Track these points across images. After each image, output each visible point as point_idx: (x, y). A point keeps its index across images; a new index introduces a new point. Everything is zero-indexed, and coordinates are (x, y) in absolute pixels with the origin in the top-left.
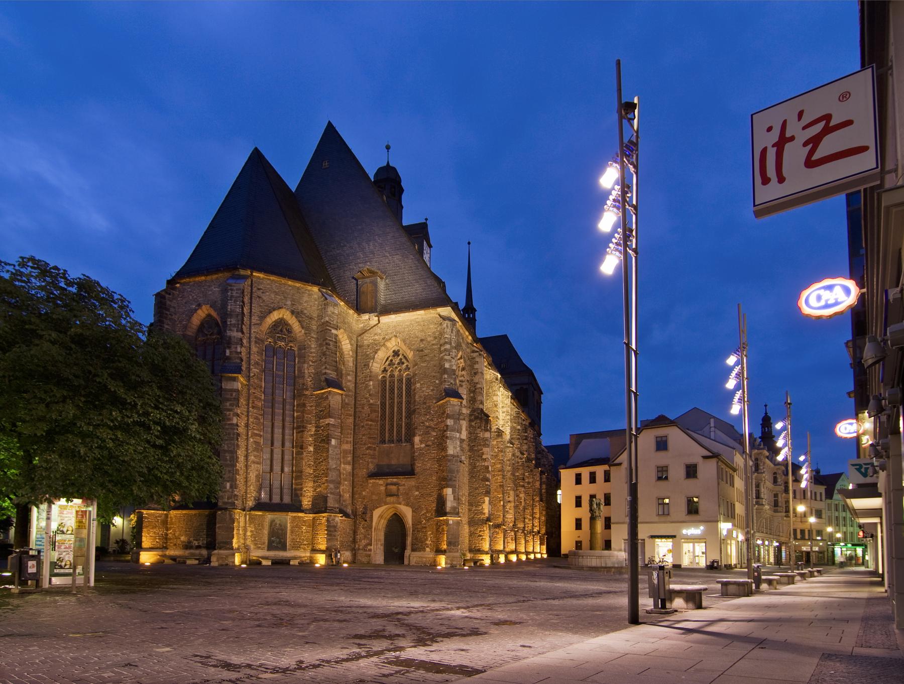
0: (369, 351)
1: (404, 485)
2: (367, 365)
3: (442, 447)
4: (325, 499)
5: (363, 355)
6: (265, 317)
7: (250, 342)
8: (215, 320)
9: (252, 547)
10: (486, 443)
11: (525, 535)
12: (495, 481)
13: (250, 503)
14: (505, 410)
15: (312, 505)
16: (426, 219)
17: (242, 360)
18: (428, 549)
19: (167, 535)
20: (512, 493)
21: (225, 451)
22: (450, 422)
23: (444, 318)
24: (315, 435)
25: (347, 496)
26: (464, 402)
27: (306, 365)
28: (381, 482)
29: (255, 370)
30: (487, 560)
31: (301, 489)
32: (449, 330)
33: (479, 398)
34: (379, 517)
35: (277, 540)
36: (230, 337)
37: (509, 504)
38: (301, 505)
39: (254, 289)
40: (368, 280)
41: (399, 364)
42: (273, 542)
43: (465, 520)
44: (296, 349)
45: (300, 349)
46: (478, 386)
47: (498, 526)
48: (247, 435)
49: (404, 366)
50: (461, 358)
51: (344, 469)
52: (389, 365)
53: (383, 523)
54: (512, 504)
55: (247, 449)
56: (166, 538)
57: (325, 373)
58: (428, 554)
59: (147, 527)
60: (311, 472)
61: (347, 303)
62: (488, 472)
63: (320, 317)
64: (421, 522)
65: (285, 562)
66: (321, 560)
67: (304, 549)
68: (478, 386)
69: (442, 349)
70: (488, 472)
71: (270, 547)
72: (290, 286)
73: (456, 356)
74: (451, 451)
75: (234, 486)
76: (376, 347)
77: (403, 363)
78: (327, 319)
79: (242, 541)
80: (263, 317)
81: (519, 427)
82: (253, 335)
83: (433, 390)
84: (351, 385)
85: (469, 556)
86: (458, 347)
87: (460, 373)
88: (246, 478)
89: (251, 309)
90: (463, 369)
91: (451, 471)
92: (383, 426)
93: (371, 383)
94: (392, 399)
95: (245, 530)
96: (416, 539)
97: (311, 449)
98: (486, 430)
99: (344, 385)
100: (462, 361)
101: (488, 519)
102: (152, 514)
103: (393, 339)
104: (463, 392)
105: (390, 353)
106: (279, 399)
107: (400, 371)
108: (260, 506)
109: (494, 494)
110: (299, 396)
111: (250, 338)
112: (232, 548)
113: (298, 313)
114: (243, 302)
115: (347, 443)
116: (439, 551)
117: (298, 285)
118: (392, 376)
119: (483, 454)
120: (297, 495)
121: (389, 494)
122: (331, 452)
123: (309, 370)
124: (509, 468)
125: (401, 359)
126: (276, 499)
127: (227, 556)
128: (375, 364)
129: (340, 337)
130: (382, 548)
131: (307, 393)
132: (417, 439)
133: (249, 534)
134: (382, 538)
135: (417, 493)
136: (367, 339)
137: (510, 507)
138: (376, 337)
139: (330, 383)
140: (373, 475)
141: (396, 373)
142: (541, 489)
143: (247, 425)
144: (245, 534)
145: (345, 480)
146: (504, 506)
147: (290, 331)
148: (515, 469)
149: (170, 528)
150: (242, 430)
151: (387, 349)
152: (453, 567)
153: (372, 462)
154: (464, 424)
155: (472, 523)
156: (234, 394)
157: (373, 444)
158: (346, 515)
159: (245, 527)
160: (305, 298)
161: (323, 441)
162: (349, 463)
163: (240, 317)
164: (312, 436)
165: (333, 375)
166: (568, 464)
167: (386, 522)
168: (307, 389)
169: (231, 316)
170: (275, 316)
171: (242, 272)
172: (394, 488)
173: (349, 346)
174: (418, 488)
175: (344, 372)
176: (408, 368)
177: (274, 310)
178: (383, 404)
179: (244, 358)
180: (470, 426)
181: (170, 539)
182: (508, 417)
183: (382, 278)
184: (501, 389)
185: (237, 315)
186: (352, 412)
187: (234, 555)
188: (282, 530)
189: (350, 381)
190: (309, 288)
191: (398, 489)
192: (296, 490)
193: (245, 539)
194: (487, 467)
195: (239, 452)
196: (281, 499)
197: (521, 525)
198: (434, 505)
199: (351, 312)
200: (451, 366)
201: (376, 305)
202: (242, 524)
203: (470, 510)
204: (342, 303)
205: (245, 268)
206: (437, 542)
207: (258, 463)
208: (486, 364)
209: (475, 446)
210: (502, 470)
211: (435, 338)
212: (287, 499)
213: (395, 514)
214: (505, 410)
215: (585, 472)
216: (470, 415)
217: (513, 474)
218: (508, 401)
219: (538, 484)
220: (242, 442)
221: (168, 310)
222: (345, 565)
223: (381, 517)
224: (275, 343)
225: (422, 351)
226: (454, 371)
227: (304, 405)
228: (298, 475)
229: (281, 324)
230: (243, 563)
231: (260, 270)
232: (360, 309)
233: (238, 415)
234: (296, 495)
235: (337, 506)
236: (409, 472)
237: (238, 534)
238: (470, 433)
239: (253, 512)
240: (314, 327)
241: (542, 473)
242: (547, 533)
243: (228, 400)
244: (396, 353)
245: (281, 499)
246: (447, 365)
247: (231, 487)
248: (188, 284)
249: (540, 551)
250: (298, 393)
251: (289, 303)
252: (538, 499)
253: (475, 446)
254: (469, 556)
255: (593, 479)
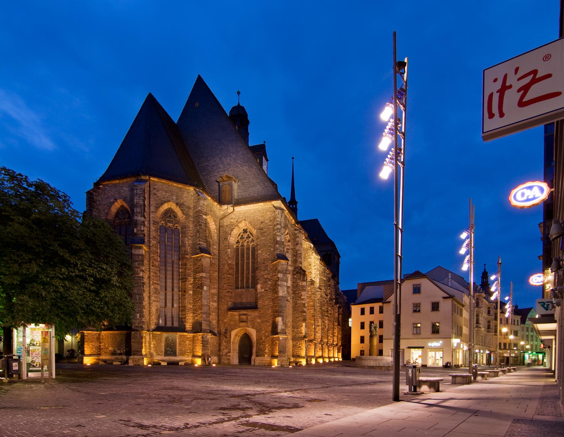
0: (228, 230)
1: (251, 315)
2: (226, 239)
3: (277, 292)
4: (200, 324)
5: (223, 232)
6: (159, 207)
7: (149, 224)
8: (126, 209)
9: (155, 354)
10: (303, 289)
11: (328, 347)
12: (309, 313)
13: (153, 327)
14: (316, 267)
15: (192, 328)
16: (265, 142)
17: (145, 236)
18: (266, 355)
19: (100, 346)
20: (320, 320)
21: (136, 294)
22: (280, 275)
23: (276, 208)
24: (193, 283)
25: (214, 322)
26: (290, 263)
27: (186, 239)
28: (236, 313)
29: (153, 242)
30: (304, 362)
31: (185, 318)
32: (279, 216)
33: (299, 260)
34: (235, 335)
35: (170, 349)
36: (136, 220)
37: (318, 327)
38: (185, 328)
39: (152, 189)
40: (226, 183)
41: (247, 238)
42: (168, 351)
43: (290, 337)
44: (179, 228)
45: (182, 228)
46: (299, 252)
47: (311, 341)
48: (150, 284)
49: (250, 239)
50: (287, 234)
51: (212, 305)
52: (241, 238)
53: (238, 339)
54: (320, 327)
55: (150, 293)
56: (99, 348)
57: (199, 244)
58: (267, 358)
59: (87, 341)
60: (191, 307)
61: (213, 198)
62: (305, 307)
63: (195, 207)
64: (262, 339)
65: (176, 363)
66: (199, 362)
67: (188, 355)
68: (299, 252)
69: (275, 228)
70: (305, 307)
71: (166, 354)
72: (175, 186)
73: (284, 233)
74: (281, 294)
75: (142, 316)
76: (232, 227)
77: (250, 237)
78: (200, 208)
79: (148, 350)
80: (157, 208)
81: (325, 279)
82: (151, 219)
83: (269, 255)
84: (216, 252)
85: (292, 359)
86: (286, 227)
87: (287, 244)
88: (150, 311)
89: (150, 202)
90: (289, 241)
91: (281, 307)
92: (237, 278)
93: (229, 250)
94: (243, 260)
95: (150, 344)
96: (259, 349)
97: (191, 292)
98: (304, 281)
99: (211, 251)
100: (288, 236)
101: (305, 337)
102: (91, 334)
103: (243, 221)
104: (289, 256)
105: (241, 231)
106: (169, 260)
107: (248, 242)
108: (159, 328)
109: (308, 321)
110: (182, 259)
111: (149, 221)
112: (142, 355)
113: (181, 204)
114: (144, 197)
115: (214, 288)
116: (274, 357)
117: (180, 186)
118: (243, 246)
119: (301, 295)
120: (182, 322)
121: (242, 321)
122: (203, 294)
123: (188, 242)
124: (318, 305)
125: (248, 235)
126: (169, 324)
127: (139, 360)
128: (231, 238)
129: (209, 220)
130: (237, 354)
131: (187, 256)
132: (259, 286)
133: (152, 346)
134: (237, 348)
135: (259, 320)
136: (226, 222)
137: (319, 329)
138: (232, 220)
139: (203, 250)
140: (231, 309)
141: (245, 244)
142: (338, 318)
143: (149, 277)
144: (150, 346)
145: (213, 312)
146: (315, 328)
147: (175, 216)
148: (322, 305)
149: (102, 342)
150: (146, 280)
151: (239, 228)
152: (282, 366)
153: (230, 301)
154: (289, 277)
155: (294, 339)
156: (140, 257)
157: (231, 289)
158: (214, 334)
159: (150, 341)
160: (185, 195)
161: (198, 287)
162: (215, 302)
163: (142, 207)
164: (191, 284)
165: (204, 245)
166: (356, 302)
167: (239, 338)
168: (187, 254)
169: (136, 206)
170: (166, 206)
171: (143, 177)
172: (244, 317)
173: (214, 226)
174: (260, 317)
175: (211, 243)
176: (253, 241)
177: (165, 202)
178: (237, 264)
179: (146, 234)
180: (293, 278)
181: (102, 349)
182: (318, 272)
183: (235, 182)
184: (314, 254)
185: (141, 206)
186: (217, 269)
187: (143, 359)
188: (173, 343)
189: (215, 249)
190: (188, 188)
191: (247, 318)
192: (181, 318)
193: (150, 349)
194: (304, 304)
195: (144, 294)
196: (173, 324)
197: (325, 340)
198: (270, 328)
199: (216, 204)
200: (281, 239)
201: (232, 199)
202: (148, 340)
203: (293, 331)
204: (209, 198)
205: (145, 174)
206: (272, 350)
207: (157, 302)
208: (304, 238)
209: (296, 290)
210: (314, 306)
211: (271, 221)
212: (176, 324)
213: (245, 333)
214: (316, 267)
215: (367, 307)
216: (294, 271)
217: (321, 308)
218: (318, 262)
219: (336, 315)
220: (146, 288)
221: (95, 202)
222: (214, 365)
223: (236, 335)
224: (166, 224)
225: (262, 229)
226: (283, 242)
227: (186, 264)
228: (183, 309)
229: (169, 213)
230: (149, 363)
231: (155, 176)
232: (221, 202)
233: (143, 271)
234: (182, 321)
235: (208, 328)
236: (254, 307)
237: (146, 346)
238: (293, 282)
239: (154, 332)
240: (192, 214)
241: (339, 307)
242: (342, 345)
243: (137, 261)
244: (245, 231)
245: (173, 324)
246: (278, 239)
247: (140, 316)
248: (108, 185)
249: (337, 356)
250: (182, 257)
251: (174, 198)
252: (336, 324)
253: (296, 290)
254: (292, 359)
255: (372, 311)
